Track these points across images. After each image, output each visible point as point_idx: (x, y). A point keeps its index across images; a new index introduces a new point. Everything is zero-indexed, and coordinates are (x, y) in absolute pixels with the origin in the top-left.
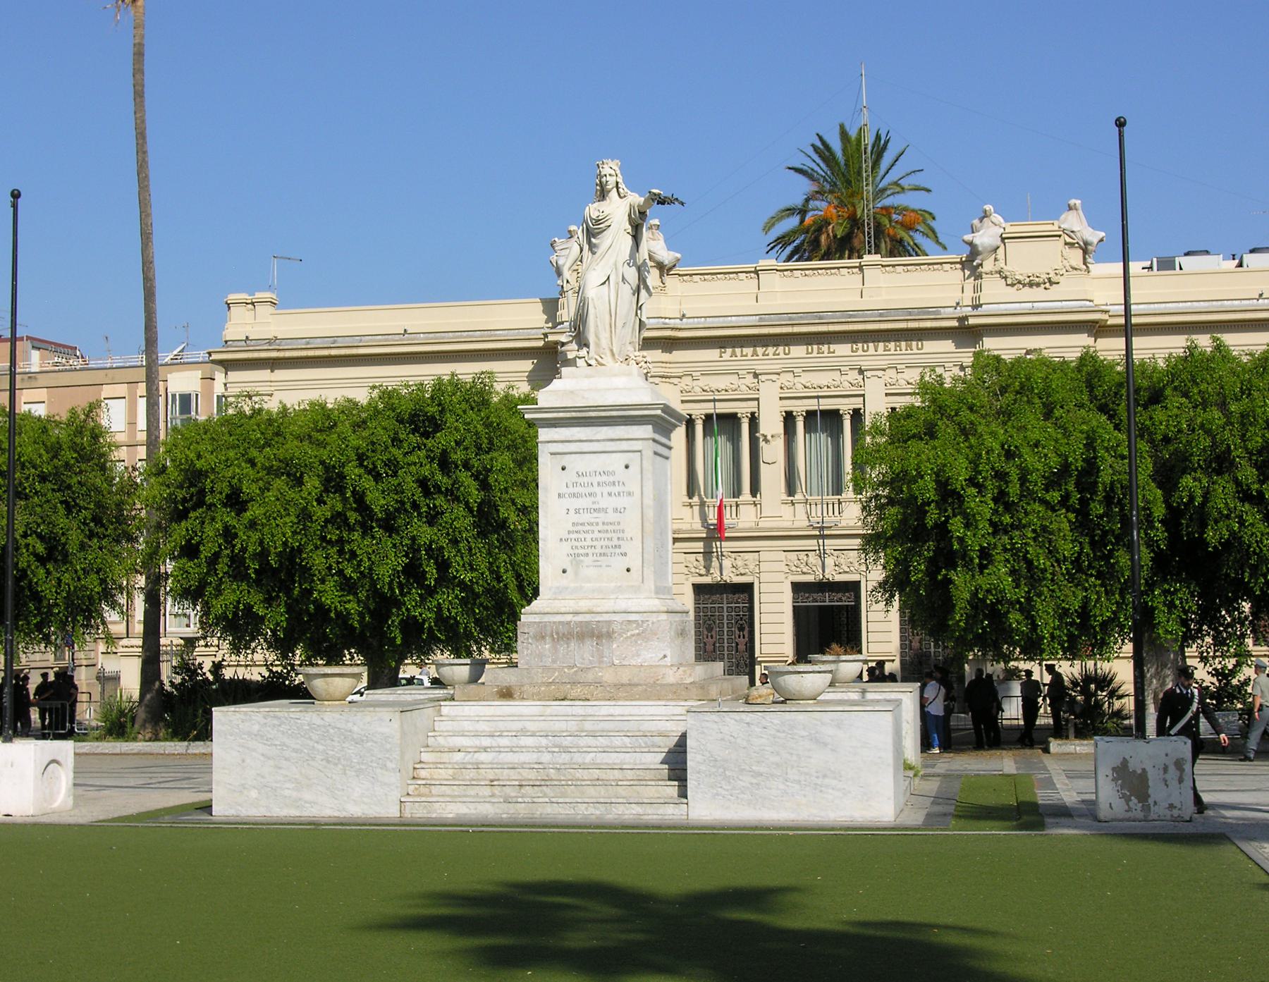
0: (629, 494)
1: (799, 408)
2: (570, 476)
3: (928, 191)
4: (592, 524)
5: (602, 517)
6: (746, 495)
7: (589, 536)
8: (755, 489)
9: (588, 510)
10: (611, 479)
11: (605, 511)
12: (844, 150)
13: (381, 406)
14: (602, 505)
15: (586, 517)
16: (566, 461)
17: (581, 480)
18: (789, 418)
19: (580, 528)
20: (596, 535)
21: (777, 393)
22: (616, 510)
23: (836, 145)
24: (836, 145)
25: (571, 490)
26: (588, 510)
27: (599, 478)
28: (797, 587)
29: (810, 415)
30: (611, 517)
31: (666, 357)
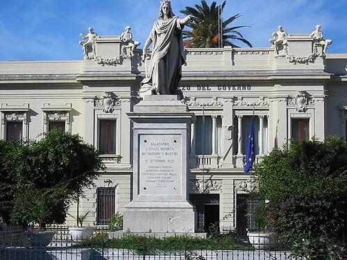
2: (148, 145)
4: (157, 167)
15: (155, 164)
17: (154, 147)
19: (152, 169)
20: (160, 172)
22: (169, 161)
27: (162, 147)
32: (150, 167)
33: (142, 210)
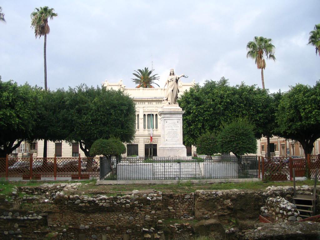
0: (178, 127)
1: (146, 114)
2: (168, 123)
3: (134, 74)
5: (173, 131)
6: (155, 128)
7: (171, 134)
8: (157, 128)
9: (171, 129)
10: (175, 124)
11: (174, 130)
12: (145, 70)
13: (67, 103)
14: (173, 129)
15: (170, 131)
16: (167, 121)
17: (170, 124)
18: (145, 115)
21: (143, 111)
23: (147, 68)
24: (147, 68)
25: (168, 126)
26: (171, 129)
28: (146, 145)
29: (148, 115)
30: (175, 131)
31: (150, 105)
32: (169, 132)
33: (167, 148)
